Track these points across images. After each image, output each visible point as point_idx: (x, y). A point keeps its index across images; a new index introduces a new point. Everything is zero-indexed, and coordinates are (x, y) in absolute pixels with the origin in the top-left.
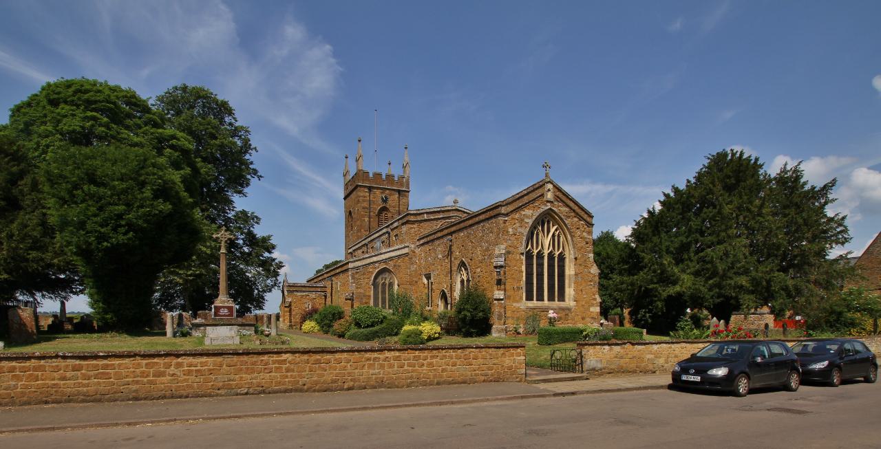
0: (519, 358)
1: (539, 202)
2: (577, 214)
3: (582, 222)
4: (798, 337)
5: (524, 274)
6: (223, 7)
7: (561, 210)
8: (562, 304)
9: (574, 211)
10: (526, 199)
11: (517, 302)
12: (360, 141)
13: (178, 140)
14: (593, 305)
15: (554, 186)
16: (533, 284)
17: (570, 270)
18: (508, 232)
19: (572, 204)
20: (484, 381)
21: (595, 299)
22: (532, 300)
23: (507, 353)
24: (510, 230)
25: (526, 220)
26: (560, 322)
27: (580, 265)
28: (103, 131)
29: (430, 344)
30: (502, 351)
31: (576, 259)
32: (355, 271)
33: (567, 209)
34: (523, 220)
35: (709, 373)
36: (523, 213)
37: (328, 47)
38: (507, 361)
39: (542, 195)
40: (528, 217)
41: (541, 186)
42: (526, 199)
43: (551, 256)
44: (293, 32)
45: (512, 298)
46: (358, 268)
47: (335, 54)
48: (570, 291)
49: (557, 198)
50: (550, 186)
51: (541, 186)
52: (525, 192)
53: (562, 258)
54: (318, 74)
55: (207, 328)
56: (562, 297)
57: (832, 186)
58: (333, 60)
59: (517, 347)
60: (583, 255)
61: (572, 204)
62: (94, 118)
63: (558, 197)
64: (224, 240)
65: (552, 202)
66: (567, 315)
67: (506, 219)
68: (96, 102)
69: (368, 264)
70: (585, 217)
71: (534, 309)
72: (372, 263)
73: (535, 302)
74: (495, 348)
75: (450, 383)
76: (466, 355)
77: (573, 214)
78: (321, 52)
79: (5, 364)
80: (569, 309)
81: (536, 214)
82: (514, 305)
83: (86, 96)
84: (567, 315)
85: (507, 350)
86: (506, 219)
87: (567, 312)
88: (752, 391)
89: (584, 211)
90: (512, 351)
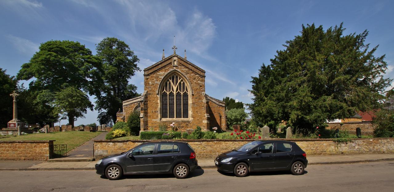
0: (45, 148)
1: (168, 67)
2: (193, 71)
3: (197, 76)
4: (315, 138)
5: (159, 105)
6: (171, 11)
7: (181, 70)
8: (186, 119)
9: (191, 70)
10: (160, 66)
11: (154, 118)
12: (164, 50)
13: (91, 59)
14: (204, 120)
15: (178, 58)
16: (167, 109)
17: (190, 101)
18: (149, 84)
19: (190, 67)
20: (25, 159)
21: (205, 116)
22: (181, 118)
23: (38, 146)
24: (150, 83)
25: (160, 77)
26: (183, 129)
27: (196, 98)
28: (53, 59)
29: (116, 139)
30: (34, 144)
31: (193, 95)
32: (125, 107)
33: (187, 69)
34: (158, 77)
35: (222, 161)
36: (158, 73)
37: (210, 19)
38: (38, 150)
39: (171, 63)
40: (161, 75)
41: (170, 59)
42: (160, 66)
43: (178, 94)
44: (197, 16)
45: (151, 117)
46: (127, 105)
47: (213, 22)
48: (190, 112)
49: (180, 64)
50: (175, 58)
51: (170, 59)
52: (160, 63)
53: (186, 95)
54: (207, 30)
55: (8, 132)
56: (186, 115)
57: (365, 36)
58: (212, 24)
59: (44, 143)
60: (198, 93)
61: (190, 67)
62: (50, 54)
63: (180, 63)
64: (14, 96)
65: (177, 66)
66: (188, 125)
67: (148, 77)
68: (53, 48)
69: (131, 103)
70: (199, 72)
71: (166, 122)
72: (133, 103)
73: (175, 118)
74: (30, 143)
75: (5, 160)
76: (13, 146)
77: (191, 72)
78: (209, 21)
79: (1, 145)
80: (189, 122)
81: (166, 73)
82: (153, 120)
83: (50, 47)
84: (188, 125)
85: (38, 144)
86: (148, 77)
87: (188, 123)
88: (248, 174)
89: (200, 70)
90: (41, 144)
